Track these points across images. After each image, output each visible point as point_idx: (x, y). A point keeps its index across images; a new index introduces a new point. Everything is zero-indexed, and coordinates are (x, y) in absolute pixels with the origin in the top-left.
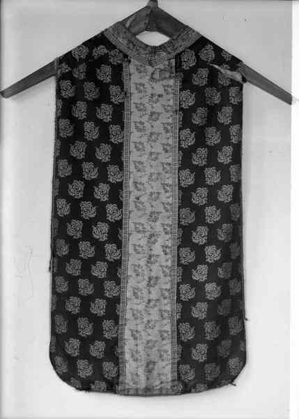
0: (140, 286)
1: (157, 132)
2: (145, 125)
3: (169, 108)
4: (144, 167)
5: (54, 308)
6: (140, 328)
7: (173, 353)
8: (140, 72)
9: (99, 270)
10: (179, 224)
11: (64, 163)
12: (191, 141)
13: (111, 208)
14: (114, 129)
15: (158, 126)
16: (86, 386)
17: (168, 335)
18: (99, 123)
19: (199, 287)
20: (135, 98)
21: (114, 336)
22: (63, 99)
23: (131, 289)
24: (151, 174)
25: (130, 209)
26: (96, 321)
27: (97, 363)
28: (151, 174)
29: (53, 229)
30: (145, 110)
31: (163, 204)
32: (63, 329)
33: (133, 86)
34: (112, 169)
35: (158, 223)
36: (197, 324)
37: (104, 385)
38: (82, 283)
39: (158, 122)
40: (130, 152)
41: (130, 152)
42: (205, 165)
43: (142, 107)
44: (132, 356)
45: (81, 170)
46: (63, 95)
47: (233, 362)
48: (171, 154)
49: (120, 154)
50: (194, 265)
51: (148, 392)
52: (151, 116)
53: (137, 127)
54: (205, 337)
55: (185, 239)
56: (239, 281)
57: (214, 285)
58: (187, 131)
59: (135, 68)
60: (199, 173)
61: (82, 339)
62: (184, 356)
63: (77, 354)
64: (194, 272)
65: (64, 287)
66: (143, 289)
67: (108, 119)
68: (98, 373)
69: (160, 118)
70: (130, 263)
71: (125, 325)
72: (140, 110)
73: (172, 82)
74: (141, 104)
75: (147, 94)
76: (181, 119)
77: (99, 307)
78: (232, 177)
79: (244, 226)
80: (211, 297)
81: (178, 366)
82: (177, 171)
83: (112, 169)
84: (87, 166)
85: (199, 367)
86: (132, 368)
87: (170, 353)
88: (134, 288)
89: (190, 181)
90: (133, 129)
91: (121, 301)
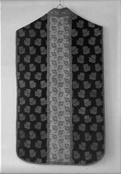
0: (55, 25)
1: (61, 47)
2: (57, 99)
3: (67, 37)
4: (57, 157)
5: (18, 128)
6: (57, 143)
7: (71, 146)
8: (54, 30)
9: (38, 110)
10: (72, 88)
11: (21, 132)
12: (76, 52)
13: (42, 32)
14: (42, 49)
15: (62, 45)
16: (33, 160)
17: (69, 157)
18: (36, 47)
19: (81, 117)
20: (52, 50)
21: (45, 54)
22: (20, 121)
23: (52, 117)
24: (59, 66)
25: (50, 73)
26: (38, 116)
27: (38, 151)
28: (59, 66)
29: (18, 93)
30: (56, 73)
31: (65, 107)
32: (23, 136)
33: (51, 27)
34: (42, 66)
35: (63, 97)
36: (81, 117)
37: (40, 160)
38: (31, 116)
39: (63, 116)
40: (50, 48)
41: (50, 48)
42: (82, 28)
43: (55, 146)
44: (53, 146)
45: (29, 153)
46: (20, 70)
47: (99, 153)
48: (69, 103)
49: (46, 93)
50: (79, 107)
51: (59, 163)
52: (60, 103)
53: (52, 46)
54: (85, 139)
55: (75, 95)
56: (101, 83)
57: (89, 153)
58: (76, 116)
59: (52, 20)
60: (80, 48)
61: (31, 140)
62: (76, 147)
63: (29, 112)
64: (79, 110)
65: (23, 102)
66: (57, 155)
67: (83, 97)
68: (38, 155)
69: (63, 59)
70: (51, 106)
71: (50, 132)
72: (54, 21)
73: (68, 26)
74: (55, 135)
75: (57, 48)
76: (73, 111)
77: (38, 126)
78: (96, 86)
79: (106, 126)
80: (86, 71)
81: (73, 151)
82: (72, 132)
83: (42, 66)
84: (31, 116)
85: (82, 153)
86: (52, 152)
87: (69, 145)
88: (53, 144)
89: (76, 34)
90: (51, 46)
91: (48, 122)
